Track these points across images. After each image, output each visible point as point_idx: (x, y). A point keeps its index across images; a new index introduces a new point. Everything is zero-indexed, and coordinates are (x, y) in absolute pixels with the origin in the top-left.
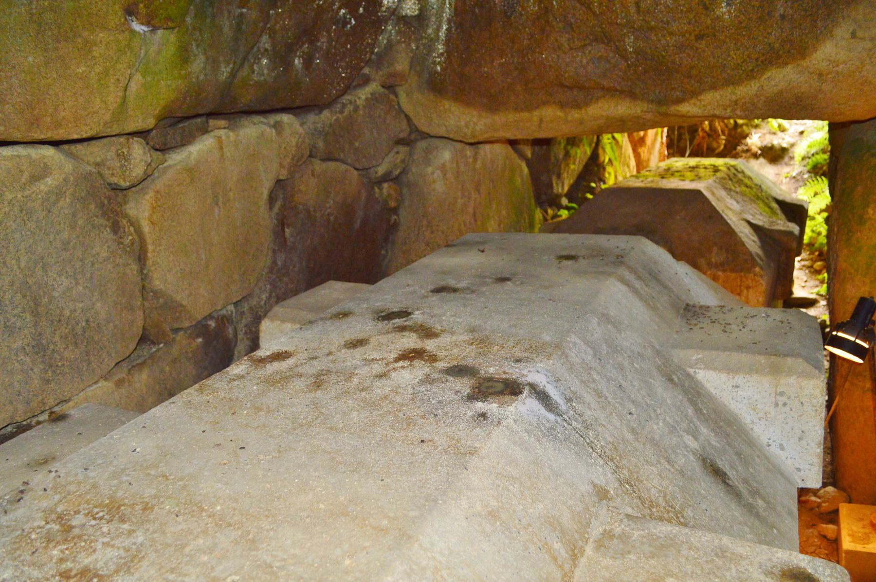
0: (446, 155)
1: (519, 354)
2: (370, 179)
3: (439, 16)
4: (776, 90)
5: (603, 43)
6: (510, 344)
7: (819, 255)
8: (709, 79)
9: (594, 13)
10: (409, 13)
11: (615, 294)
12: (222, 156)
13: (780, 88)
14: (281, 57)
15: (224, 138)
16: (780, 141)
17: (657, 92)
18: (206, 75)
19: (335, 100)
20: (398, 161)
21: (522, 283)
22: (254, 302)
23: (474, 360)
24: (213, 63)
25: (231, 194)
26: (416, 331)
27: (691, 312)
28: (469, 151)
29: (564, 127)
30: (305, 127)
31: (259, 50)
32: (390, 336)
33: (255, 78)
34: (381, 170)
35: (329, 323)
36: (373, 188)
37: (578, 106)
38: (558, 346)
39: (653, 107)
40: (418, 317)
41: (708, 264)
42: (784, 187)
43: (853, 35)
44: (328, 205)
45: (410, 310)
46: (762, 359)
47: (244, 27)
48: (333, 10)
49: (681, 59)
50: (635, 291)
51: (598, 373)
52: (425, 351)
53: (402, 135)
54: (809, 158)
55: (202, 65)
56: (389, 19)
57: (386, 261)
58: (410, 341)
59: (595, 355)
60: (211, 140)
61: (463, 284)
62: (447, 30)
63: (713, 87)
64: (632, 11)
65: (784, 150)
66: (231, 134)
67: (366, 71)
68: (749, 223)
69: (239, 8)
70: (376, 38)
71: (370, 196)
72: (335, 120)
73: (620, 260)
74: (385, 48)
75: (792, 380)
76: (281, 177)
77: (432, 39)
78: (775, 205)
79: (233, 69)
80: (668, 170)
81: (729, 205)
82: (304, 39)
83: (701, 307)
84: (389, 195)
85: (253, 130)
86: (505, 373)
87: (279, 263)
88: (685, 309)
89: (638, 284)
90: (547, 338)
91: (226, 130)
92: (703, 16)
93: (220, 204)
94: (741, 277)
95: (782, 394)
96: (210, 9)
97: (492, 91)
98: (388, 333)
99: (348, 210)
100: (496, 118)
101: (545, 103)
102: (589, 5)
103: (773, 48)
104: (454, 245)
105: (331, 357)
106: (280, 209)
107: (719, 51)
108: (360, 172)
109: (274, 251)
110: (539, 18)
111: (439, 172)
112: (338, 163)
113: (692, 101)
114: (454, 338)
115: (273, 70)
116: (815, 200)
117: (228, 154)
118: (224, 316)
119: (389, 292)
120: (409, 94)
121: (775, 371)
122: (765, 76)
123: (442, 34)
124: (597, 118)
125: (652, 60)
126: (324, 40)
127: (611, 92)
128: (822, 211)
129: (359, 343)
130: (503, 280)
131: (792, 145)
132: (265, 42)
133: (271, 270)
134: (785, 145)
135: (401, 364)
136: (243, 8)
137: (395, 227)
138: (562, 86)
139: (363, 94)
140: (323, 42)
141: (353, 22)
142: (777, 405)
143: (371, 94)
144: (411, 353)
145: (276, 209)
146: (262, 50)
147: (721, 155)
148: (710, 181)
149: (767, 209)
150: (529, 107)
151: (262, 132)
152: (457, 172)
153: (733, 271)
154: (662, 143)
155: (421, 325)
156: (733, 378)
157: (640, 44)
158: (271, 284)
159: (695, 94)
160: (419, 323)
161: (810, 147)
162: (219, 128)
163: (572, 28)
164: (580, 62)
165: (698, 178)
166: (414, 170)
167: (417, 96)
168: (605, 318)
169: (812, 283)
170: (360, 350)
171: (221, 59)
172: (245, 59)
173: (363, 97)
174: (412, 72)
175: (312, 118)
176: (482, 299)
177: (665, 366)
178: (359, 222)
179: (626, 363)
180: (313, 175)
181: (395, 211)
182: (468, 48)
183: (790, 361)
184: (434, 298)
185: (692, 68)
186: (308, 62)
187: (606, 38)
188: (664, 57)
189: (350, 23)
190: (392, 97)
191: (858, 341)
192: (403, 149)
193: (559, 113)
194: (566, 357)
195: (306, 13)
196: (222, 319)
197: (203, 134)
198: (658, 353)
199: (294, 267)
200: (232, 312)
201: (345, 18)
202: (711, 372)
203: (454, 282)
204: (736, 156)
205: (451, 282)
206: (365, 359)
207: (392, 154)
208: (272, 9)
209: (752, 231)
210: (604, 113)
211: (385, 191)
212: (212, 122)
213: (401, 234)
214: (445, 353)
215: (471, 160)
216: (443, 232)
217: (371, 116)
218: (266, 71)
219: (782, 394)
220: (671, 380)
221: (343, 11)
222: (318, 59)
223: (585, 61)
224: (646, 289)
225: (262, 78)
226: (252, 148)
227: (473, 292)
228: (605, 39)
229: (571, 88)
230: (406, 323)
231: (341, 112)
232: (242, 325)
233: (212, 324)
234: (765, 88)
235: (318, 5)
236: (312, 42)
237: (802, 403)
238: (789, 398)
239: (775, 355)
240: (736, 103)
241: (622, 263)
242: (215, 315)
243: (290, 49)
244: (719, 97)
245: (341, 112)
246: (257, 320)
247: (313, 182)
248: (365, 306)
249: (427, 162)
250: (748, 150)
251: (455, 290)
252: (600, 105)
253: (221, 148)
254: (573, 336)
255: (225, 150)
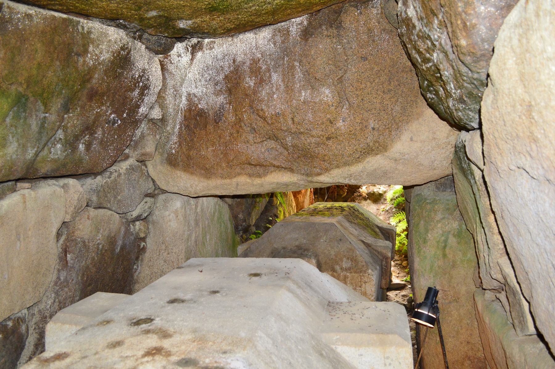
0: (177, 203)
1: (225, 347)
2: (127, 219)
3: (175, 121)
4: (372, 168)
5: (274, 140)
6: (219, 340)
7: (405, 257)
8: (335, 162)
9: (268, 123)
10: (156, 117)
11: (286, 301)
12: (25, 207)
13: (374, 167)
14: (71, 144)
15: (27, 195)
16: (378, 190)
17: (306, 169)
18: (17, 155)
19: (105, 170)
20: (147, 207)
21: (226, 295)
22: (42, 306)
23: (196, 353)
24: (24, 147)
25: (30, 233)
26: (156, 333)
27: (331, 306)
28: (192, 201)
29: (252, 188)
30: (84, 187)
31: (55, 139)
32: (139, 338)
33: (52, 156)
34: (135, 214)
35: (96, 329)
36: (129, 225)
37: (259, 176)
38: (250, 340)
39: (304, 177)
40: (158, 322)
41: (341, 269)
42: (381, 218)
43: (411, 139)
44: (98, 238)
45: (152, 318)
46: (374, 337)
47: (46, 125)
48: (106, 115)
49: (318, 150)
50: (297, 296)
51: (276, 356)
52: (162, 349)
53: (149, 192)
54: (395, 199)
55: (15, 149)
56: (143, 120)
57: (137, 273)
58: (153, 341)
59: (274, 343)
60: (18, 197)
61: (188, 297)
62: (179, 128)
63: (338, 167)
64: (290, 123)
65: (381, 195)
66: (32, 193)
67: (127, 151)
68: (363, 242)
69: (44, 113)
70: (134, 132)
71: (127, 230)
72: (105, 183)
73: (287, 276)
74: (140, 137)
75: (393, 349)
76: (66, 220)
77: (170, 134)
78: (377, 230)
79: (37, 151)
80: (315, 210)
81: (351, 232)
82: (87, 132)
83: (337, 303)
84: (140, 229)
85: (48, 189)
86: (216, 362)
87: (62, 278)
88: (328, 305)
89: (299, 291)
90: (243, 334)
91: (29, 190)
92: (330, 127)
93: (21, 239)
94: (361, 276)
95: (388, 358)
96: (24, 114)
97: (207, 166)
98: (137, 335)
99: (112, 241)
100: (210, 182)
101: (239, 174)
102: (265, 119)
103: (369, 146)
104: (183, 267)
105: (97, 356)
106: (64, 241)
107: (340, 146)
108: (121, 215)
109: (59, 271)
110: (235, 124)
111: (173, 217)
112: (106, 210)
113: (326, 174)
114: (182, 337)
115: (64, 152)
116: (399, 224)
117: (30, 206)
118: (19, 318)
119: (138, 303)
120: (154, 166)
121: (383, 344)
122: (366, 161)
123: (177, 129)
124: (272, 184)
125: (302, 150)
126: (100, 133)
127: (279, 168)
128: (404, 230)
129: (117, 344)
130: (215, 292)
131: (385, 192)
132: (60, 134)
133: (56, 284)
134: (381, 192)
135: (146, 359)
136: (46, 113)
137: (144, 249)
138: (250, 164)
139: (124, 166)
140: (99, 134)
141: (119, 122)
142: (385, 365)
143: (130, 166)
144: (153, 350)
145: (61, 241)
146: (58, 139)
147: (345, 201)
148: (340, 217)
149: (373, 233)
150: (230, 177)
151: (54, 191)
152: (185, 215)
153: (355, 272)
154: (311, 192)
155: (160, 329)
156: (359, 350)
157: (295, 141)
158: (55, 293)
159: (327, 170)
160: (159, 327)
161: (395, 193)
162: (24, 189)
163: (255, 131)
164: (258, 150)
165: (332, 215)
166: (157, 213)
167: (160, 167)
168: (280, 317)
169: (402, 274)
170: (118, 349)
171: (29, 145)
172: (46, 144)
173: (124, 168)
174: (157, 152)
175: (91, 182)
176: (201, 307)
177: (318, 346)
178: (119, 248)
179: (293, 347)
180: (88, 218)
181: (144, 239)
182: (193, 140)
183: (391, 337)
184: (169, 308)
185: (325, 155)
186: (88, 147)
187: (275, 137)
188: (309, 149)
189: (117, 123)
190: (143, 167)
191: (429, 314)
192: (148, 199)
193: (248, 180)
194: (256, 347)
195: (89, 117)
196: (18, 320)
197: (12, 193)
198: (313, 337)
199: (73, 280)
200: (25, 314)
201: (114, 120)
202: (345, 347)
203: (182, 295)
204: (353, 200)
205: (180, 295)
206: (121, 357)
207: (143, 203)
208: (66, 114)
209: (365, 247)
210: (275, 181)
211: (137, 227)
212: (19, 185)
213: (147, 255)
214: (176, 349)
215: (194, 207)
216: (175, 253)
217: (129, 180)
218: (59, 152)
219: (388, 358)
220: (321, 355)
221: (113, 116)
222: (95, 144)
223: (263, 150)
224: (304, 294)
225: (57, 157)
226: (46, 202)
227: (195, 302)
228: (275, 138)
229: (255, 166)
230: (150, 328)
231: (109, 177)
232: (33, 323)
233: (10, 324)
234: (367, 167)
235: (97, 112)
236: (91, 134)
237: (400, 363)
238: (392, 360)
239: (382, 333)
240: (351, 176)
241: (288, 278)
242: (13, 317)
243: (77, 138)
244: (341, 172)
245: (109, 177)
246: (45, 319)
247: (89, 222)
248: (122, 315)
249: (165, 207)
250: (361, 195)
251: (183, 301)
252: (273, 175)
253: (25, 202)
254: (259, 332)
255: (27, 203)
